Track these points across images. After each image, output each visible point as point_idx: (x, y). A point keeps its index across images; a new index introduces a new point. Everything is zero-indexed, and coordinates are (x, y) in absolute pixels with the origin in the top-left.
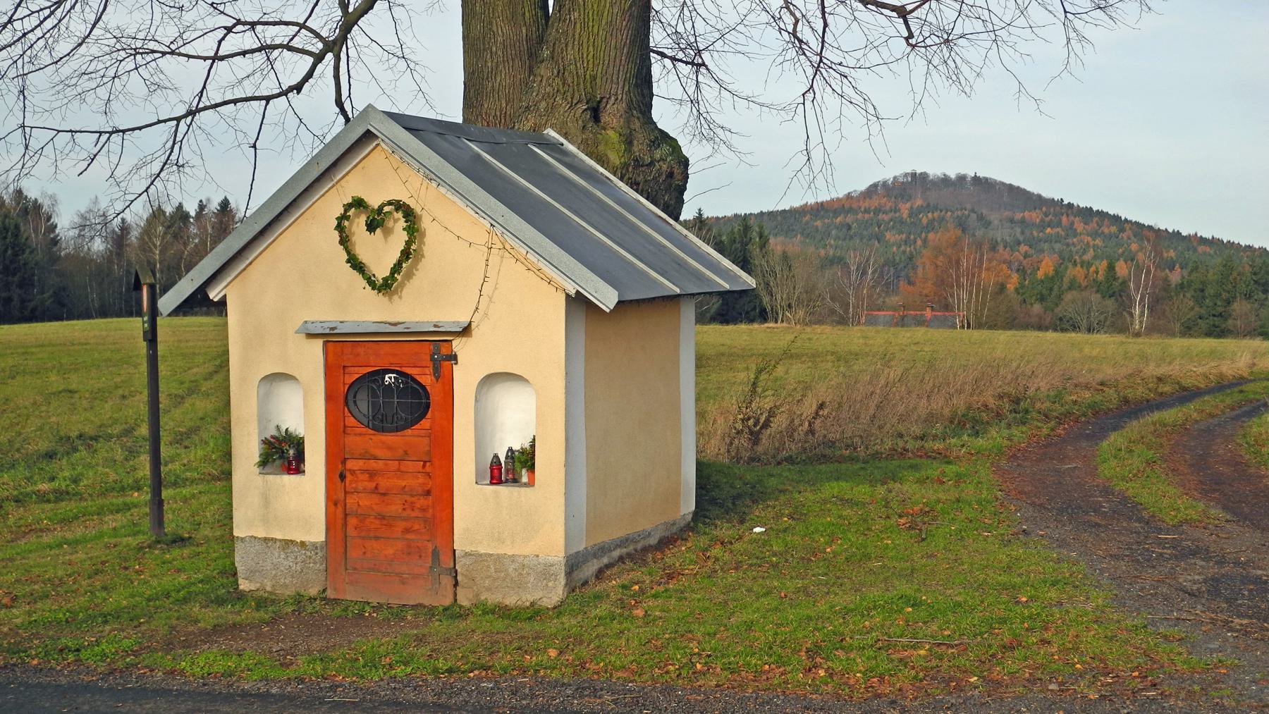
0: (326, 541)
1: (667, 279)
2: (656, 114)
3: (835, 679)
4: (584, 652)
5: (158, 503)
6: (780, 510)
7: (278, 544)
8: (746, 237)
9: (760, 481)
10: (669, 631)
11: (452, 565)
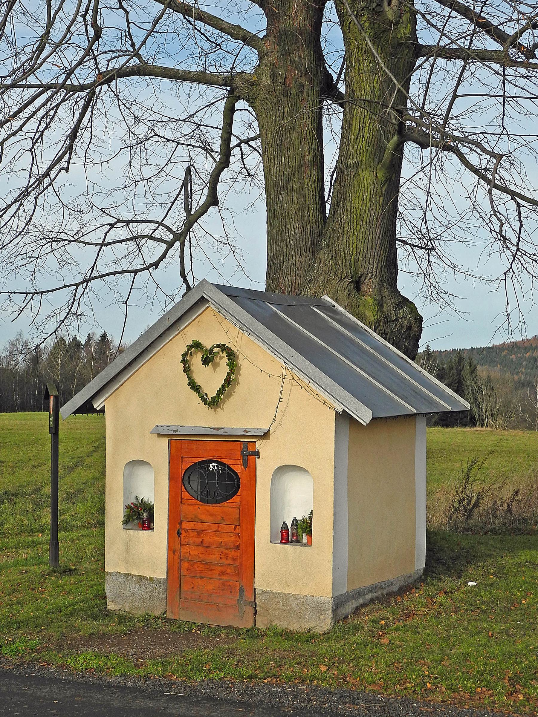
0: (167, 578)
1: (408, 403)
2: (399, 286)
3: (531, 702)
4: (346, 668)
5: (55, 543)
6: (487, 570)
7: (134, 578)
8: (460, 365)
9: (472, 547)
10: (407, 657)
11: (253, 600)
